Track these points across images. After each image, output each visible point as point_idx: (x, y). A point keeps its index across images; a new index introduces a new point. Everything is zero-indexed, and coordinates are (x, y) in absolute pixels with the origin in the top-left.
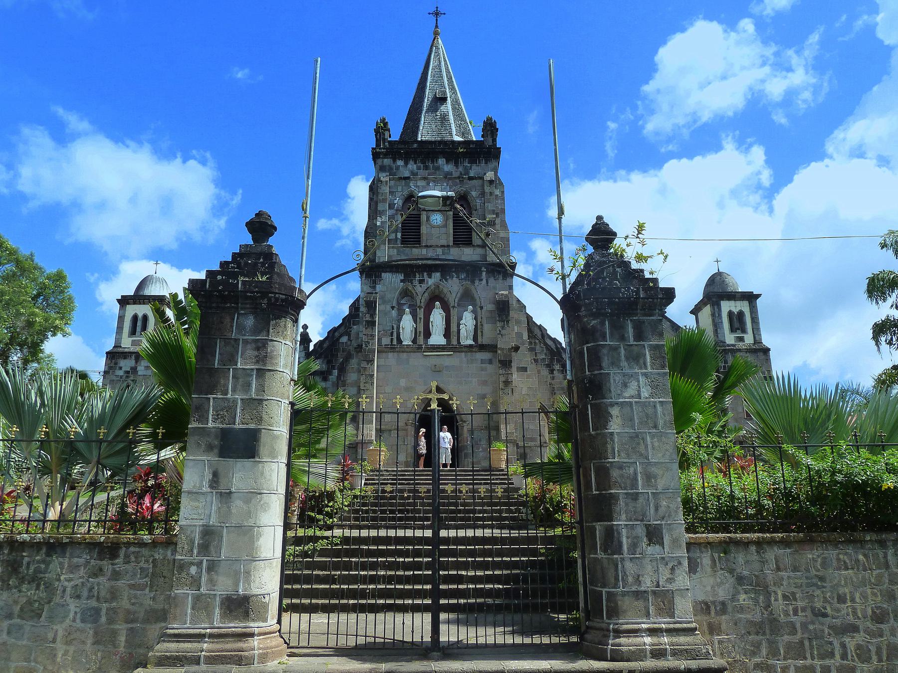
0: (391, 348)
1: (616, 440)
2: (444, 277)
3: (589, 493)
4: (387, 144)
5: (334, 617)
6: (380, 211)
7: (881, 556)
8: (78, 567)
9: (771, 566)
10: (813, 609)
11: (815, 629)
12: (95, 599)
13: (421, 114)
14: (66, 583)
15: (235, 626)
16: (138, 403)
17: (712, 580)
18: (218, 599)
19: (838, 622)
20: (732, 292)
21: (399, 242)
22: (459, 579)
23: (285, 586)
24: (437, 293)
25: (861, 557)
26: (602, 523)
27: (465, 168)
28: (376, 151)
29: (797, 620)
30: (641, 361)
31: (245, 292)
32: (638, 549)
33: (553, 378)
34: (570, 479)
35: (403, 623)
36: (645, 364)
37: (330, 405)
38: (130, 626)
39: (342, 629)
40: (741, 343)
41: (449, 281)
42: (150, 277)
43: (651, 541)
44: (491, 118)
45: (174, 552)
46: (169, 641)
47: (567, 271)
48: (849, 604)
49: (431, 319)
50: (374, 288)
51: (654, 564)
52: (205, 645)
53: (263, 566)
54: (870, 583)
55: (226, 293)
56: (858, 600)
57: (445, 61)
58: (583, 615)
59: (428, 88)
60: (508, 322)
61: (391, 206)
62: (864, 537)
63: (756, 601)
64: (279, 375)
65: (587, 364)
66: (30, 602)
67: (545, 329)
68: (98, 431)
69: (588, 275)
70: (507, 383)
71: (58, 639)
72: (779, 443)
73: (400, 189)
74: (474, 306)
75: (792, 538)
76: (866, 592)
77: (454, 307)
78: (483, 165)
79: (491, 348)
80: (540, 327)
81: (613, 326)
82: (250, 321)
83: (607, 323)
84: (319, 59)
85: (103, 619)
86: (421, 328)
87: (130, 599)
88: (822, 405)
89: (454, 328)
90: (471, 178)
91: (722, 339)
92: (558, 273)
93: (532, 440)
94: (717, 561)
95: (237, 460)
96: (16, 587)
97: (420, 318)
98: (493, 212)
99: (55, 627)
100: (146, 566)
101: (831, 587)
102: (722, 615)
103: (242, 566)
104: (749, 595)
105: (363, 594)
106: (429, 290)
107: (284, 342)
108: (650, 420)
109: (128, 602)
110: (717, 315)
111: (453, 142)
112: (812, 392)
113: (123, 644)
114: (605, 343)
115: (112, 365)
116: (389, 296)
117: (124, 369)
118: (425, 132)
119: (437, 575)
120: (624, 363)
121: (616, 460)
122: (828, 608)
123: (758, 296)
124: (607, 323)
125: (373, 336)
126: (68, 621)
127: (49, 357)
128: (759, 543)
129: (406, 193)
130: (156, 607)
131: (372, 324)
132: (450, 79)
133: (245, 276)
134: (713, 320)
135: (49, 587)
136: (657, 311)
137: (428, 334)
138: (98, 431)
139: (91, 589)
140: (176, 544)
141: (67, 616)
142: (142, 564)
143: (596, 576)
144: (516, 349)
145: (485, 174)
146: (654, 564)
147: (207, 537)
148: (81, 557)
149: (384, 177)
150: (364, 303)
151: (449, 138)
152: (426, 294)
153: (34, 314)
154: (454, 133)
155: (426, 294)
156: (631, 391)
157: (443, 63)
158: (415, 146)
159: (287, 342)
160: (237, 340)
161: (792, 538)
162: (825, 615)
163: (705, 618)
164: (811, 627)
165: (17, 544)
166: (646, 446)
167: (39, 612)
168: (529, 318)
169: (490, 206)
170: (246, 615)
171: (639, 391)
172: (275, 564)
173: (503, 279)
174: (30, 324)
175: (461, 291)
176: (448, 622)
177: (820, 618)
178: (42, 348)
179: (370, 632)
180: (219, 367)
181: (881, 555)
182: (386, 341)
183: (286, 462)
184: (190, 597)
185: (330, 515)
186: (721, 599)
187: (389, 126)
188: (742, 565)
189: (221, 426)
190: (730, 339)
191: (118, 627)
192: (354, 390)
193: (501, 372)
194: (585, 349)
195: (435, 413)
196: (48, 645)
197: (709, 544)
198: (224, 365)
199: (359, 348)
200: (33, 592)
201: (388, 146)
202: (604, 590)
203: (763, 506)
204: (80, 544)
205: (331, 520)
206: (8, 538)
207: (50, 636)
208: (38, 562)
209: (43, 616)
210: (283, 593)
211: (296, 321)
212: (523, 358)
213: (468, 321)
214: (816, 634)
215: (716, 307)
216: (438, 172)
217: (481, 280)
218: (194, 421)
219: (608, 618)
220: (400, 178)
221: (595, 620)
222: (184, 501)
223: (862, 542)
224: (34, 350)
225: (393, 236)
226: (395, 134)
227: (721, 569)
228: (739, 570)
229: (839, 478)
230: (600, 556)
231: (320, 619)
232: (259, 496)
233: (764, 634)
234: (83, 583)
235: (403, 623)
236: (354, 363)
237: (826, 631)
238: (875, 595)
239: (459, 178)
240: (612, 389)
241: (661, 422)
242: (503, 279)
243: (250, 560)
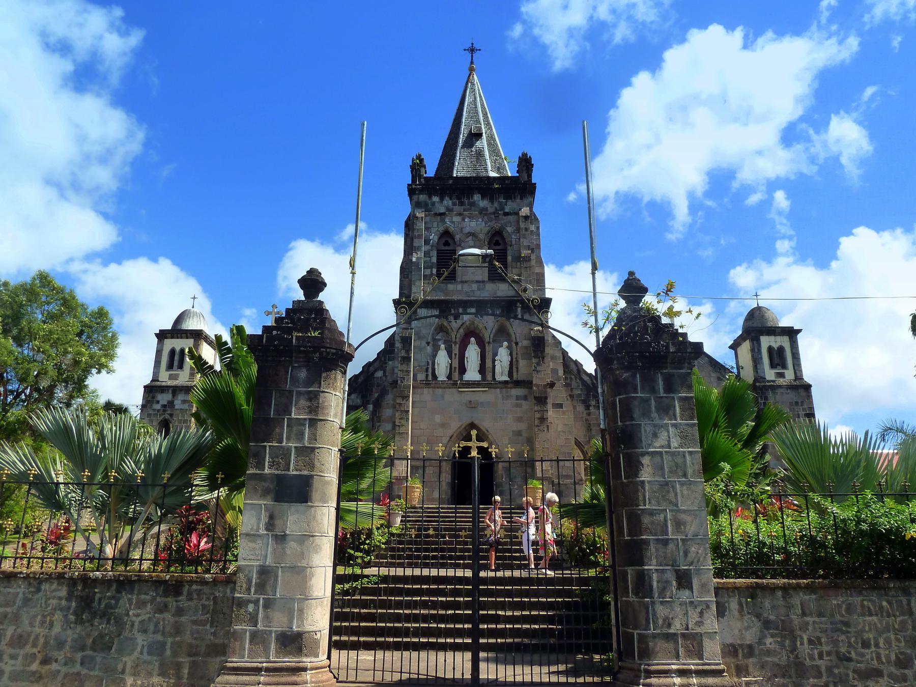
0: (427, 384)
1: (647, 488)
3: (622, 538)
4: (422, 180)
5: (380, 654)
6: (415, 247)
7: (904, 603)
8: (144, 603)
9: (797, 611)
10: (838, 653)
11: (840, 673)
12: (160, 633)
13: (456, 150)
14: (134, 619)
15: (289, 661)
16: (192, 447)
17: (739, 624)
18: (273, 635)
19: (862, 666)
20: (772, 327)
22: (496, 619)
23: (335, 624)
24: (472, 328)
25: (885, 604)
26: (633, 568)
27: (500, 203)
28: (412, 188)
29: (822, 664)
30: (671, 413)
31: (298, 346)
32: (668, 593)
33: (589, 414)
34: (603, 523)
35: (445, 661)
36: (675, 415)
37: (376, 452)
38: (192, 659)
39: (388, 666)
40: (781, 380)
42: (187, 312)
43: (680, 586)
44: (526, 154)
45: (233, 590)
46: (228, 674)
47: (601, 322)
48: (873, 649)
49: (466, 355)
51: (684, 607)
52: (262, 678)
53: (315, 605)
54: (894, 629)
55: (282, 347)
56: (881, 645)
57: (480, 96)
58: (616, 655)
59: (463, 124)
60: (543, 358)
61: (427, 242)
62: (888, 584)
63: (783, 645)
64: (328, 425)
65: (619, 415)
66: (101, 636)
67: (580, 363)
68: (163, 475)
69: (620, 330)
70: (543, 420)
71: (127, 671)
72: (805, 492)
73: (435, 224)
74: (509, 341)
75: (817, 584)
76: (890, 638)
77: (489, 343)
78: (518, 200)
79: (527, 384)
80: (576, 363)
81: (644, 379)
82: (303, 374)
83: (638, 376)
84: (366, 123)
85: (168, 652)
86: (456, 364)
87: (192, 634)
88: (852, 452)
89: (489, 364)
90: (506, 214)
91: (762, 375)
92: (591, 326)
93: (567, 477)
94: (745, 606)
95: (291, 504)
96: (89, 621)
97: (456, 354)
98: (529, 248)
99: (124, 659)
100: (207, 603)
101: (856, 632)
102: (749, 658)
103: (296, 605)
104: (775, 639)
105: (406, 632)
106: (464, 326)
107: (334, 393)
108: (680, 469)
109: (190, 636)
110: (756, 350)
111: (489, 178)
112: (842, 438)
113: (186, 676)
114: (636, 395)
115: (150, 398)
116: (424, 331)
117: (161, 403)
118: (460, 169)
119: (477, 615)
120: (654, 415)
121: (647, 507)
122: (853, 653)
123: (799, 331)
124: (638, 376)
125: (408, 372)
126: (136, 653)
127: (93, 393)
128: (785, 589)
129: (441, 229)
130: (217, 641)
131: (407, 359)
132: (485, 115)
133: (299, 332)
134: (753, 356)
135: (120, 623)
136: (686, 365)
137: (463, 370)
138: (163, 475)
139: (156, 625)
140: (235, 583)
141: (136, 649)
142: (203, 602)
143: (629, 617)
144: (552, 385)
145: (520, 209)
146: (684, 607)
147: (263, 576)
148: (147, 594)
149: (420, 214)
150: (399, 339)
151: (484, 174)
152: (461, 330)
153: (80, 353)
154: (490, 168)
155: (461, 330)
156: (661, 440)
157: (478, 99)
158: (451, 182)
159: (337, 393)
160: (291, 392)
161: (817, 584)
162: (850, 660)
163: (733, 660)
164: (836, 671)
165: (89, 581)
166: (676, 495)
167: (110, 645)
168: (565, 353)
169: (525, 242)
170: (299, 651)
171: (669, 441)
172: (325, 603)
174: (76, 363)
175: (496, 327)
176: (487, 660)
177: (845, 662)
178: (86, 383)
179: (414, 669)
180: (275, 417)
181: (905, 602)
182: (421, 376)
183: (335, 506)
184: (248, 632)
185: (368, 553)
186: (748, 643)
187: (425, 162)
188: (769, 610)
189: (276, 472)
190: (770, 374)
191: (181, 660)
192: (389, 426)
193: (536, 408)
194: (617, 401)
195: (475, 460)
196: (118, 676)
197: (736, 588)
198: (279, 415)
199: (395, 382)
200: (104, 626)
201: (423, 182)
202: (636, 632)
203: (791, 552)
204: (147, 581)
205: (369, 558)
206: (82, 576)
207: (120, 667)
208: (109, 598)
209: (113, 649)
210: (333, 631)
211: (344, 373)
212: (558, 394)
213: (503, 357)
214: (840, 678)
215: (755, 342)
218: (252, 467)
219: (640, 658)
220: (436, 214)
221: (627, 660)
222: (240, 541)
223: (886, 589)
224: (79, 386)
225: (428, 272)
226: (431, 170)
227: (749, 613)
228: (765, 615)
229: (864, 527)
230: (631, 599)
231: (366, 656)
232: (311, 538)
233: (790, 677)
234: (149, 618)
235: (445, 661)
236: (389, 398)
237: (851, 675)
238: (898, 640)
239: (494, 213)
240: (643, 439)
241: (690, 472)
243: (304, 598)
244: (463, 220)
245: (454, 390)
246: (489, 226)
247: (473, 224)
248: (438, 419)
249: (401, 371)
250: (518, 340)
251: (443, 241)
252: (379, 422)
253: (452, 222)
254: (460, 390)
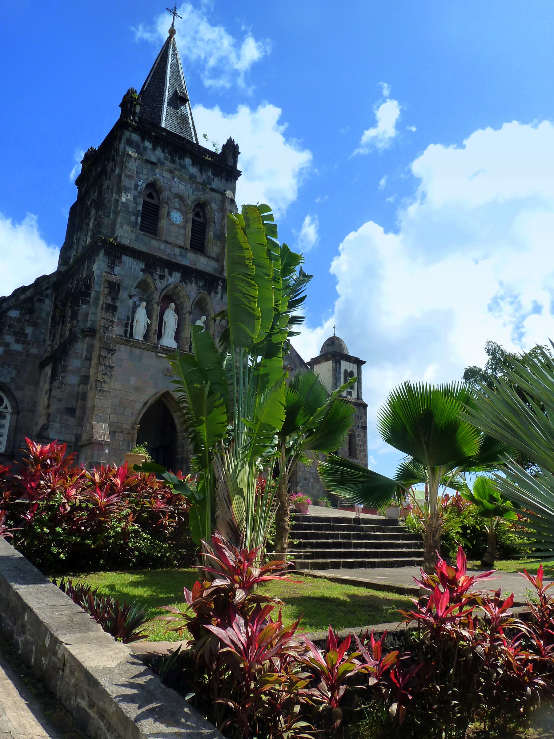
21: (138, 227)
41: (189, 285)
50: (112, 268)
59: (168, 81)
73: (145, 171)
78: (224, 181)
86: (155, 326)
90: (213, 190)
97: (157, 315)
110: (338, 371)
123: (364, 362)
129: (151, 179)
217: (216, 293)
244: (173, 178)
245: (153, 354)
246: (196, 195)
247: (182, 187)
248: (133, 381)
249: (104, 319)
251: (148, 192)
252: (64, 372)
254: (159, 354)
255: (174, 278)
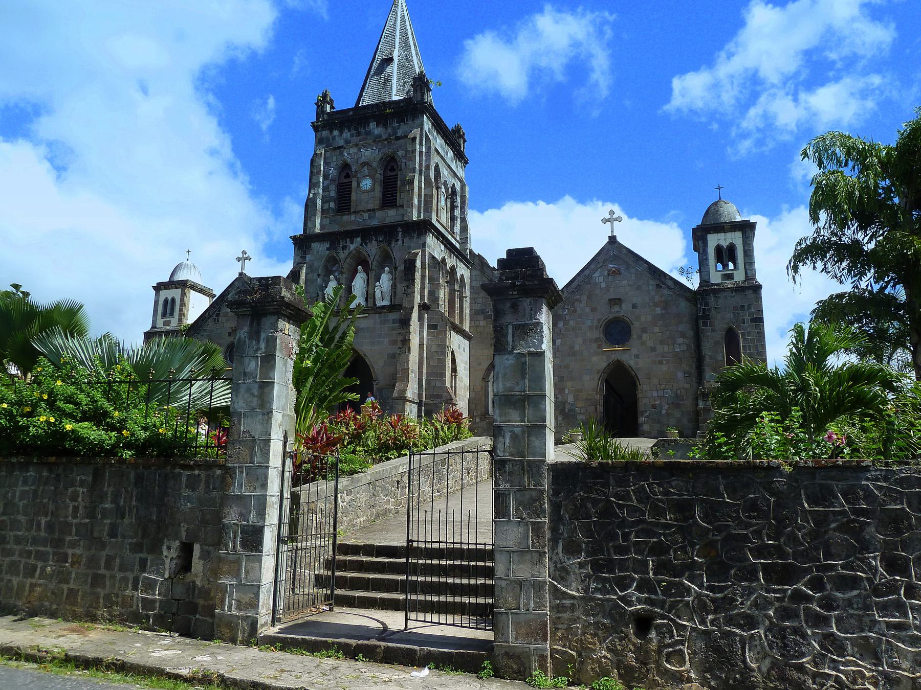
2: (364, 242)
27: (394, 128)
40: (728, 282)
50: (304, 258)
73: (334, 159)
173: (418, 238)
202: (12, 534)
216: (368, 137)
217: (397, 241)
220: (335, 148)
239: (386, 139)
242: (418, 238)
244: (359, 150)
247: (368, 153)
250: (397, 265)
251: (344, 174)
253: (348, 155)
255: (354, 245)
